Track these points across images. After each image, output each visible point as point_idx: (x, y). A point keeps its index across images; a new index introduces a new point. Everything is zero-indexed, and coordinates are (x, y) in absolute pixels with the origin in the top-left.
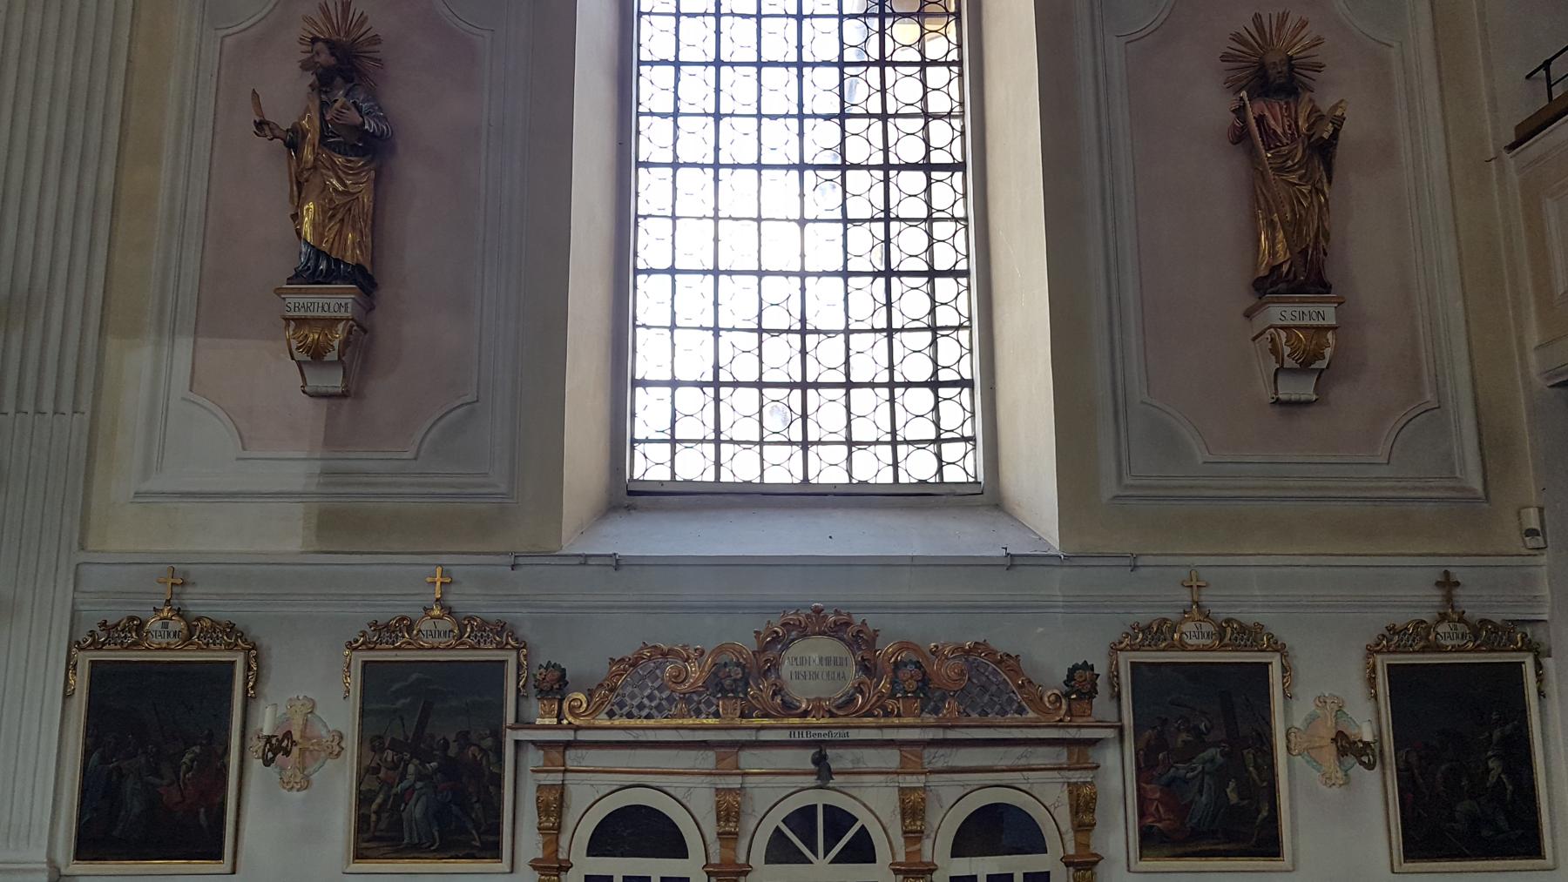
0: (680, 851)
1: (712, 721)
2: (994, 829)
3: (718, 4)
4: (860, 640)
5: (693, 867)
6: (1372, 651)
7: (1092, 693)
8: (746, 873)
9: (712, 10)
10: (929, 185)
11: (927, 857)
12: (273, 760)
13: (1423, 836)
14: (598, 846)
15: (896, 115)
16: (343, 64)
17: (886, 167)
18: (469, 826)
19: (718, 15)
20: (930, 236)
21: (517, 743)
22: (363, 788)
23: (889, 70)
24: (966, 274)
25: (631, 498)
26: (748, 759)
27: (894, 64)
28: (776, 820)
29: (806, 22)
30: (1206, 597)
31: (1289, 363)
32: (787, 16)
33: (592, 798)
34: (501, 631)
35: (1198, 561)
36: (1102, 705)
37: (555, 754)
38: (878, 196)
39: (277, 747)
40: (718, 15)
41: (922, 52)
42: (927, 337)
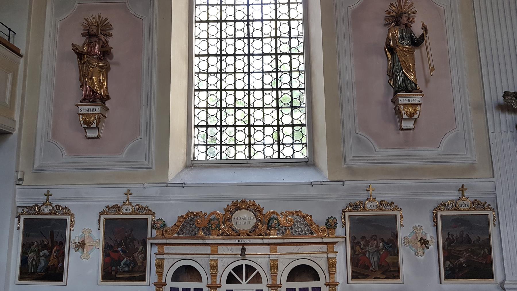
0: (200, 280)
1: (275, 236)
2: (187, 272)
3: (221, 2)
4: (257, 210)
5: (263, 286)
6: (101, 214)
7: (335, 226)
8: (220, 287)
9: (219, 3)
10: (291, 60)
11: (278, 283)
12: (78, 250)
13: (453, 272)
14: (176, 277)
15: (280, 37)
16: (399, 19)
17: (276, 54)
18: (55, 274)
19: (221, 5)
20: (291, 77)
21: (151, 244)
22: (396, 257)
23: (278, 22)
24: (196, 90)
25: (192, 165)
26: (280, 249)
27: (280, 20)
28: (230, 269)
29: (250, 7)
30: (374, 194)
31: (405, 116)
32: (244, 5)
33: (172, 262)
34: (146, 210)
35: (49, 187)
36: (339, 231)
37: (214, 248)
38: (274, 64)
39: (81, 245)
40: (221, 5)
41: (289, 16)
42: (290, 110)
